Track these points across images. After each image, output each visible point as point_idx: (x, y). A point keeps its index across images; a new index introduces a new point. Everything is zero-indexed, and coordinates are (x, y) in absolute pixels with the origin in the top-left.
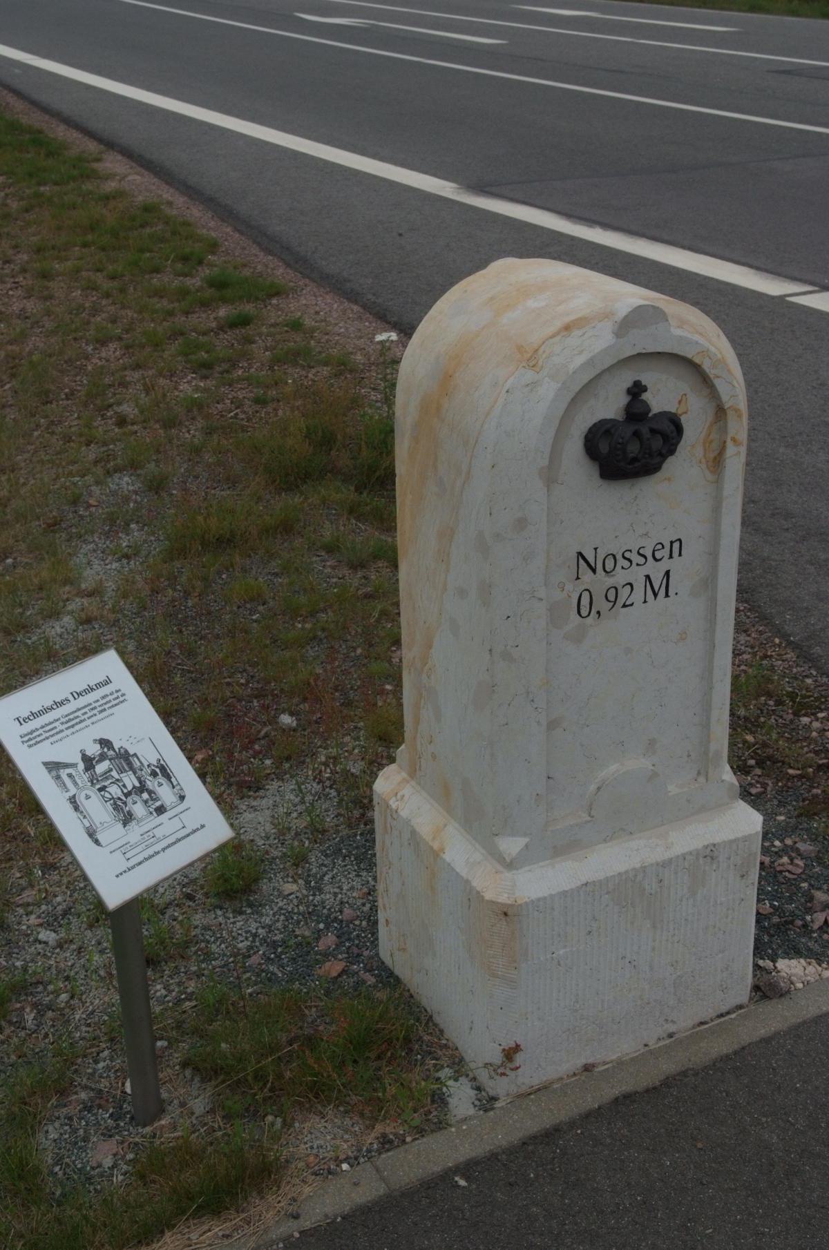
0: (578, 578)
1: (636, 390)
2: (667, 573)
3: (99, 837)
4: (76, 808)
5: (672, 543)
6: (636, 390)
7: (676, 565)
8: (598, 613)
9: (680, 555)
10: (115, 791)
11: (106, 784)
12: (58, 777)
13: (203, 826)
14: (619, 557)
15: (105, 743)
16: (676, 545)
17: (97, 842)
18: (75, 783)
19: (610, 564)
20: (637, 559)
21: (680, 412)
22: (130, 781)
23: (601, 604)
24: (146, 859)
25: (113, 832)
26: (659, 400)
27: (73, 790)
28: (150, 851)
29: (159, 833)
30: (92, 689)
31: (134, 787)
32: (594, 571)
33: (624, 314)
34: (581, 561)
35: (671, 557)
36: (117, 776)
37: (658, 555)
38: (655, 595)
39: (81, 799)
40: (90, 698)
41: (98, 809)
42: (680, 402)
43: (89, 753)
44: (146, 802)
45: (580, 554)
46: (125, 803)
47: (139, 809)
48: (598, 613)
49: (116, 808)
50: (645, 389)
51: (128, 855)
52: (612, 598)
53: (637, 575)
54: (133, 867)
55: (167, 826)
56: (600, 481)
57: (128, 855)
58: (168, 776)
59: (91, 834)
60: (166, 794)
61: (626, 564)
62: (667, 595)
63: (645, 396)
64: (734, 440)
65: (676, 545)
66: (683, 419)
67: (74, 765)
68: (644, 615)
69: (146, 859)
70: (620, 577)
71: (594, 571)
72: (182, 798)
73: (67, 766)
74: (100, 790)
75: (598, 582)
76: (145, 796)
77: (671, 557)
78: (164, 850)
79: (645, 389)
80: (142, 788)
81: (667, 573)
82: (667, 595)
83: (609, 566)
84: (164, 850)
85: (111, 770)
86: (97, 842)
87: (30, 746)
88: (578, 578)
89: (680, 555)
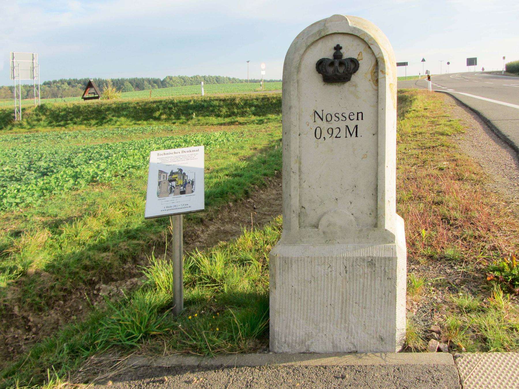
0: (346, 137)
1: (338, 48)
2: (356, 126)
4: (159, 185)
5: (358, 113)
6: (338, 48)
7: (359, 123)
8: (324, 138)
9: (362, 119)
14: (333, 116)
16: (360, 115)
19: (329, 118)
20: (341, 118)
21: (359, 58)
23: (325, 134)
26: (347, 54)
27: (162, 179)
32: (322, 120)
33: (369, 33)
34: (316, 114)
35: (358, 119)
37: (351, 117)
38: (351, 135)
39: (162, 183)
42: (359, 55)
48: (324, 138)
50: (341, 48)
52: (330, 132)
53: (342, 125)
56: (323, 83)
61: (337, 119)
62: (357, 136)
63: (342, 51)
65: (360, 115)
66: (360, 62)
67: (167, 173)
68: (345, 142)
70: (334, 124)
71: (322, 120)
72: (193, 192)
73: (165, 173)
77: (358, 119)
79: (341, 48)
82: (357, 136)
88: (346, 137)
89: (362, 119)
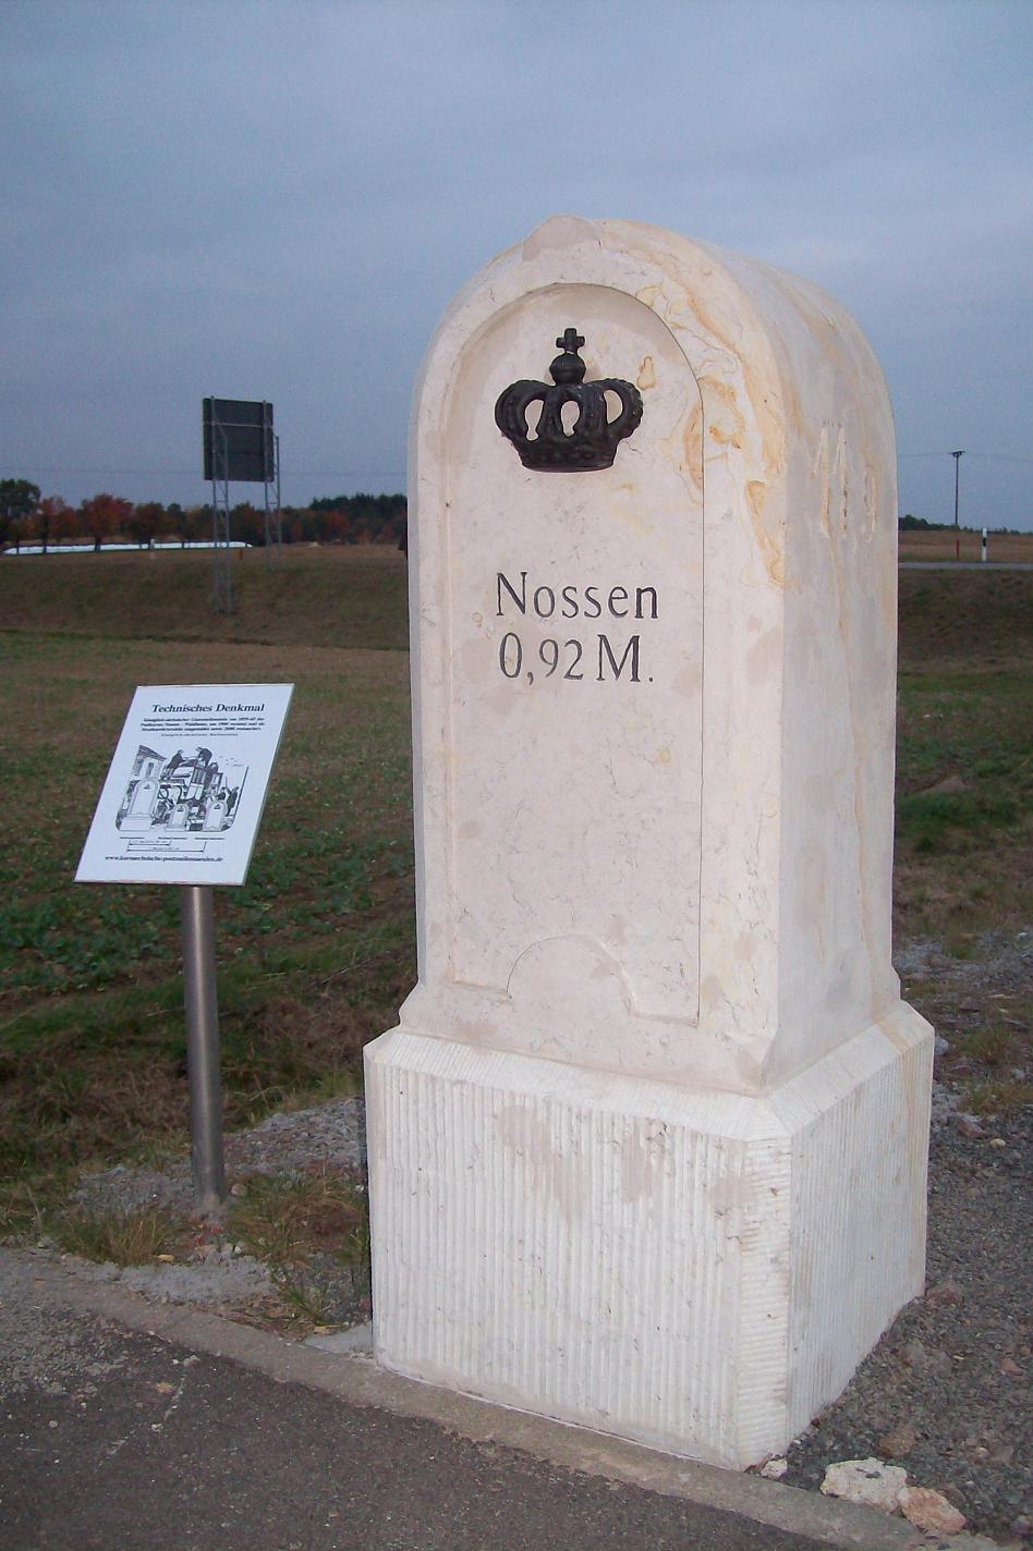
1: (571, 341)
2: (635, 640)
3: (125, 822)
5: (640, 592)
6: (571, 341)
7: (645, 628)
8: (530, 674)
9: (654, 615)
10: (174, 794)
11: (172, 784)
12: (141, 762)
13: (219, 860)
14: (558, 594)
15: (206, 754)
16: (647, 598)
17: (118, 825)
18: (149, 772)
20: (585, 605)
22: (195, 791)
23: (531, 661)
24: (143, 858)
25: (139, 824)
28: (152, 855)
29: (175, 844)
30: (240, 709)
31: (193, 798)
35: (639, 615)
36: (187, 784)
37: (619, 606)
38: (617, 672)
39: (140, 787)
40: (228, 715)
41: (146, 800)
43: (183, 756)
44: (191, 815)
45: (501, 576)
46: (172, 807)
47: (178, 817)
48: (530, 674)
49: (162, 807)
50: (580, 342)
51: (131, 847)
52: (550, 657)
54: (126, 859)
55: (192, 841)
57: (131, 847)
58: (231, 804)
59: (121, 816)
60: (215, 816)
61: (570, 610)
64: (714, 431)
65: (647, 598)
66: (644, 396)
69: (143, 858)
70: (560, 627)
72: (226, 827)
73: (156, 756)
74: (163, 787)
75: (533, 628)
76: (195, 810)
78: (165, 859)
79: (580, 342)
80: (199, 803)
81: (635, 640)
83: (545, 606)
84: (165, 859)
85: (188, 776)
86: (118, 825)
87: (144, 729)
89: (654, 615)
